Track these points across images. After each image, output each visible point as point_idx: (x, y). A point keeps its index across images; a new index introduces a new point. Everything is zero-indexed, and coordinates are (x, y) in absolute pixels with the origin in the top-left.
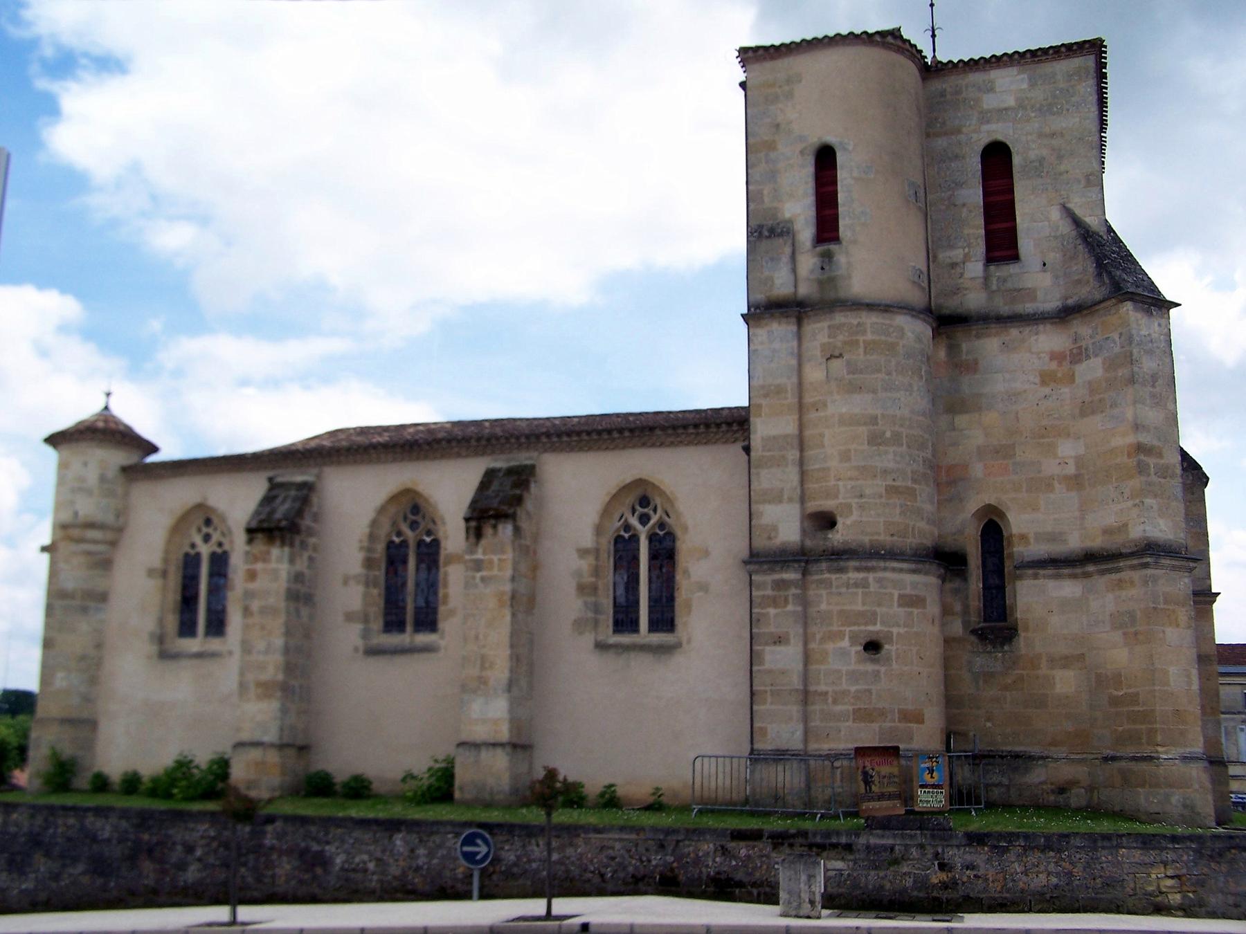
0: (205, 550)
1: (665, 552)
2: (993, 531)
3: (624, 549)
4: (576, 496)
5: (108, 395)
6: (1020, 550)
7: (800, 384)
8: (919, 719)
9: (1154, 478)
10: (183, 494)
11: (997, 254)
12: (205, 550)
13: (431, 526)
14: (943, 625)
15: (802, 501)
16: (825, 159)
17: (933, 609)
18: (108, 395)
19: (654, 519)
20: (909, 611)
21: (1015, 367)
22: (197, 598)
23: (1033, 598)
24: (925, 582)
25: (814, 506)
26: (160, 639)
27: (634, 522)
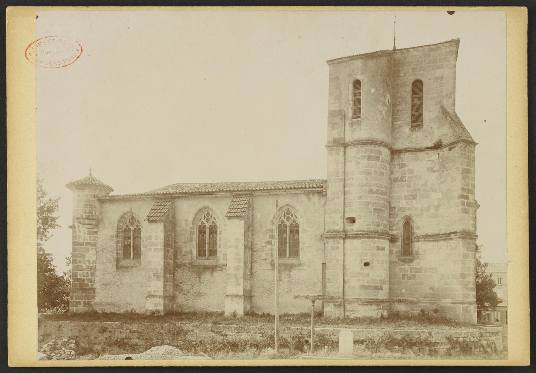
0: (208, 225)
1: (295, 230)
2: (408, 223)
3: (281, 229)
4: (267, 211)
5: (90, 170)
6: (418, 232)
7: (344, 172)
8: (381, 289)
9: (466, 207)
10: (124, 208)
11: (415, 124)
12: (208, 225)
13: (295, 219)
14: (390, 256)
15: (173, 282)
16: (357, 84)
17: (387, 252)
18: (90, 170)
19: (292, 219)
20: (381, 254)
21: (418, 166)
22: (129, 247)
23: (417, 246)
24: (385, 243)
25: (347, 215)
26: (118, 260)
27: (285, 220)
